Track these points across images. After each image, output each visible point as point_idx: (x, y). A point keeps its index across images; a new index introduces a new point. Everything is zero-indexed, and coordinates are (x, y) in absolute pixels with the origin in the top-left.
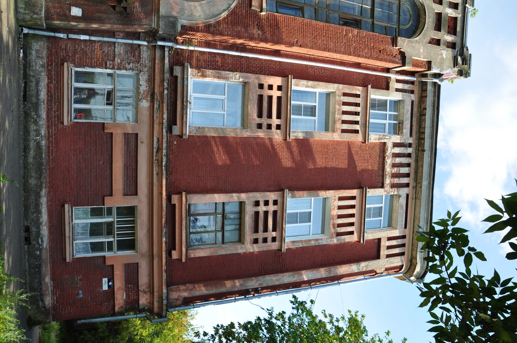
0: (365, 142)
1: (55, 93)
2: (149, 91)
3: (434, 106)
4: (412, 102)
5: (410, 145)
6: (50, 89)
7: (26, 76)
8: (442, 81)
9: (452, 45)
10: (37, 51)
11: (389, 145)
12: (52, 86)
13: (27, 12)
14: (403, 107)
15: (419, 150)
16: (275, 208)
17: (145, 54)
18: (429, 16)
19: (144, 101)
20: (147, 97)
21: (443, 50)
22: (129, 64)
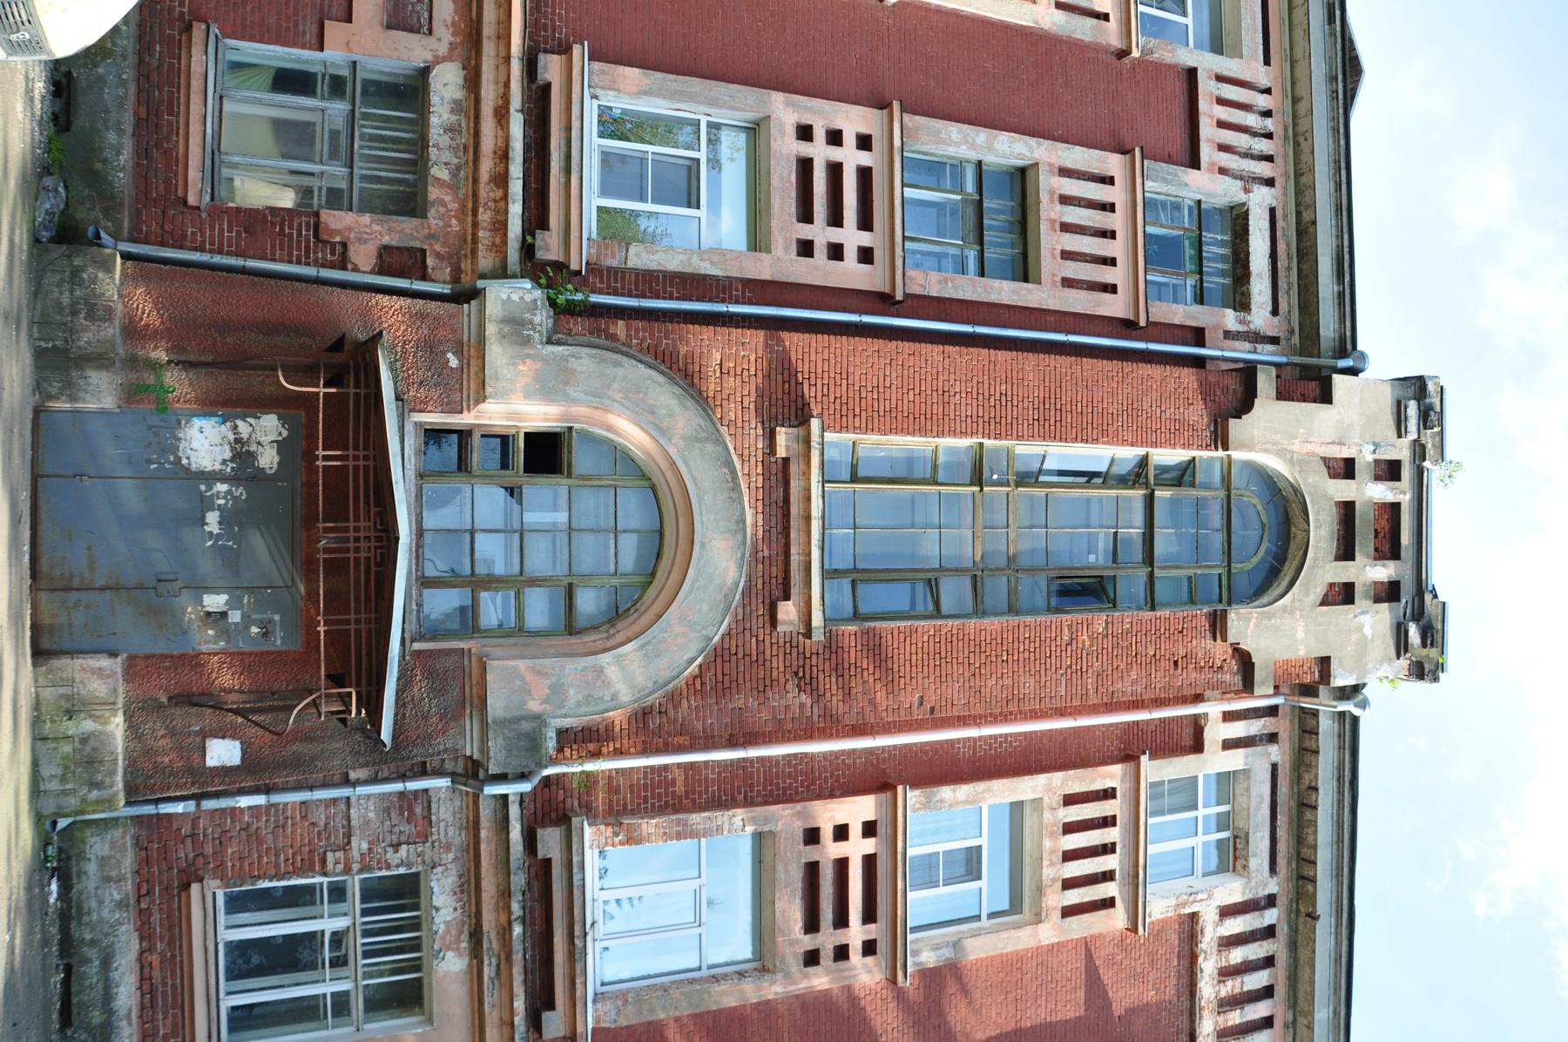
0: (1134, 930)
1: (164, 978)
2: (464, 923)
3: (1340, 779)
4: (1274, 767)
5: (1271, 901)
6: (146, 971)
7: (67, 945)
8: (1364, 705)
9: (1390, 592)
10: (103, 862)
11: (1209, 916)
12: (155, 958)
13: (69, 786)
14: (1248, 790)
15: (1298, 910)
16: (869, 846)
17: (446, 813)
18: (1317, 520)
19: (450, 955)
20: (458, 940)
21: (1363, 613)
22: (396, 847)
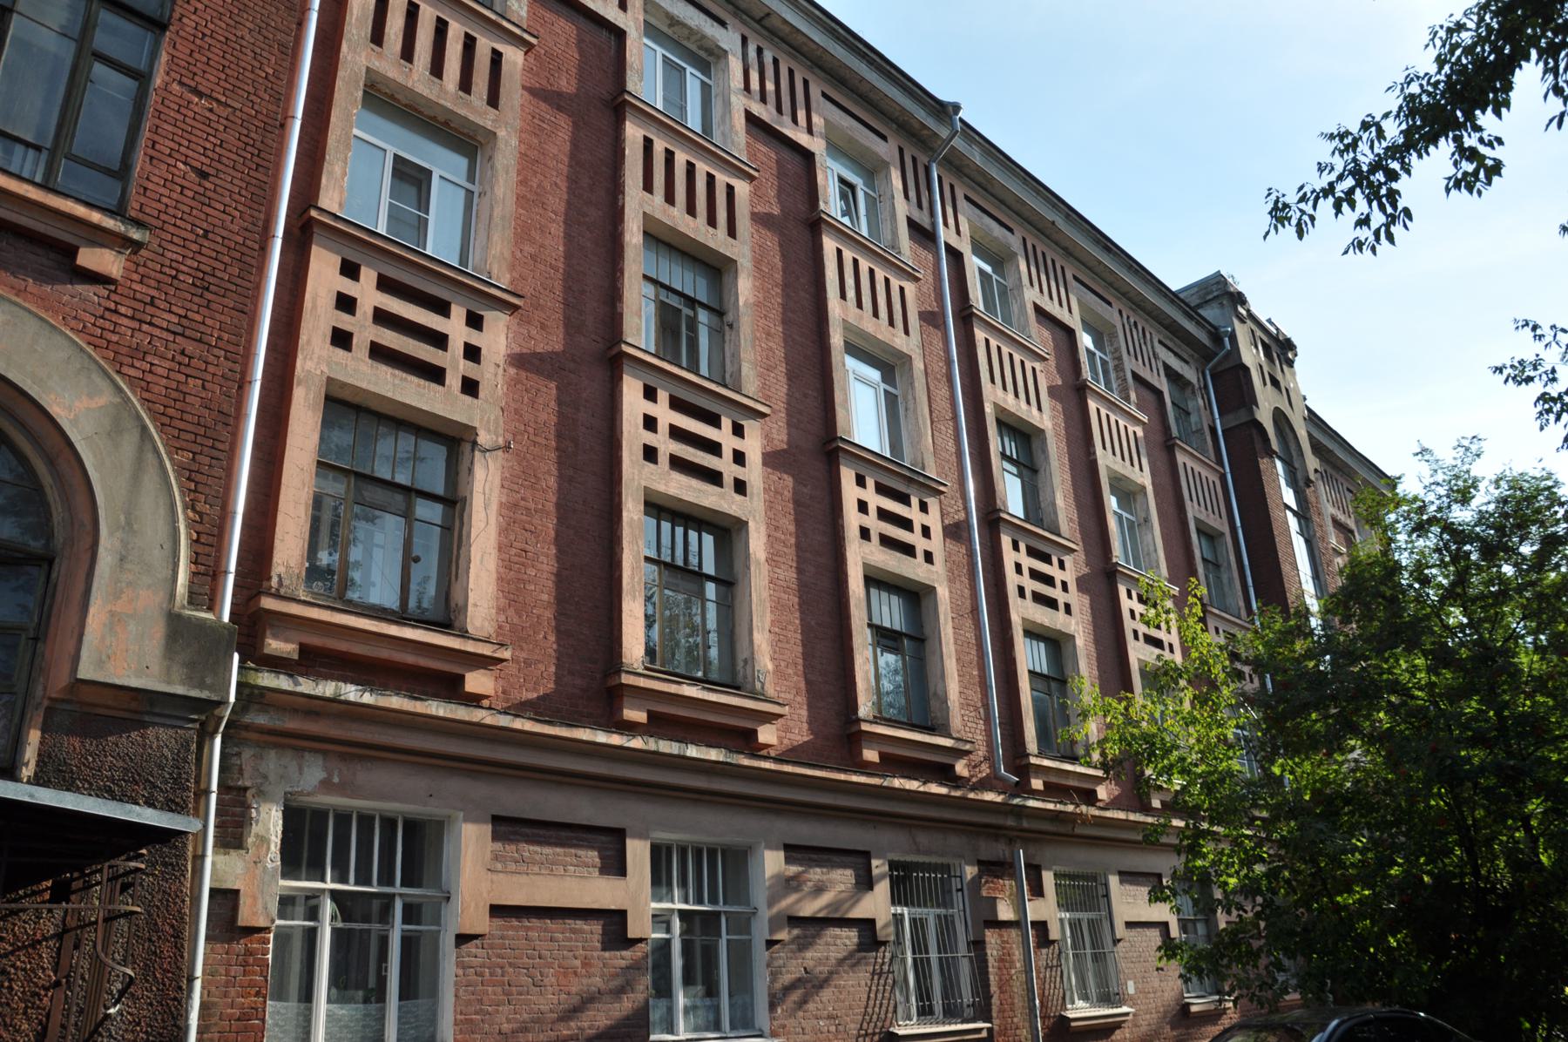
16: (368, 276)
